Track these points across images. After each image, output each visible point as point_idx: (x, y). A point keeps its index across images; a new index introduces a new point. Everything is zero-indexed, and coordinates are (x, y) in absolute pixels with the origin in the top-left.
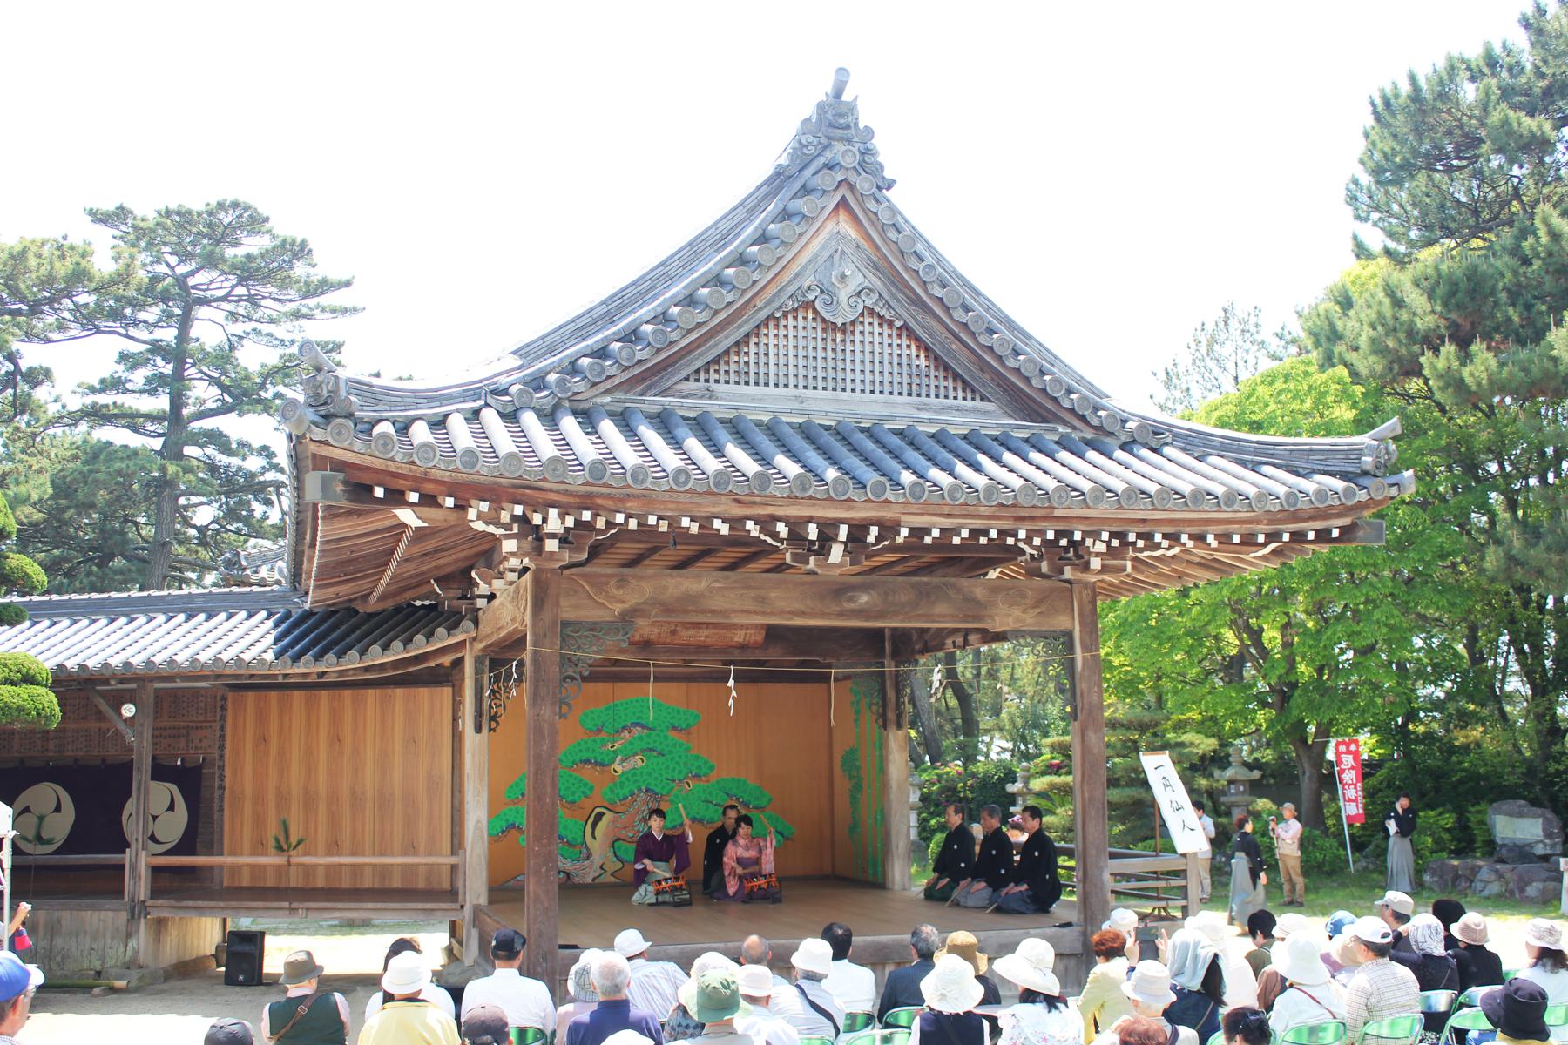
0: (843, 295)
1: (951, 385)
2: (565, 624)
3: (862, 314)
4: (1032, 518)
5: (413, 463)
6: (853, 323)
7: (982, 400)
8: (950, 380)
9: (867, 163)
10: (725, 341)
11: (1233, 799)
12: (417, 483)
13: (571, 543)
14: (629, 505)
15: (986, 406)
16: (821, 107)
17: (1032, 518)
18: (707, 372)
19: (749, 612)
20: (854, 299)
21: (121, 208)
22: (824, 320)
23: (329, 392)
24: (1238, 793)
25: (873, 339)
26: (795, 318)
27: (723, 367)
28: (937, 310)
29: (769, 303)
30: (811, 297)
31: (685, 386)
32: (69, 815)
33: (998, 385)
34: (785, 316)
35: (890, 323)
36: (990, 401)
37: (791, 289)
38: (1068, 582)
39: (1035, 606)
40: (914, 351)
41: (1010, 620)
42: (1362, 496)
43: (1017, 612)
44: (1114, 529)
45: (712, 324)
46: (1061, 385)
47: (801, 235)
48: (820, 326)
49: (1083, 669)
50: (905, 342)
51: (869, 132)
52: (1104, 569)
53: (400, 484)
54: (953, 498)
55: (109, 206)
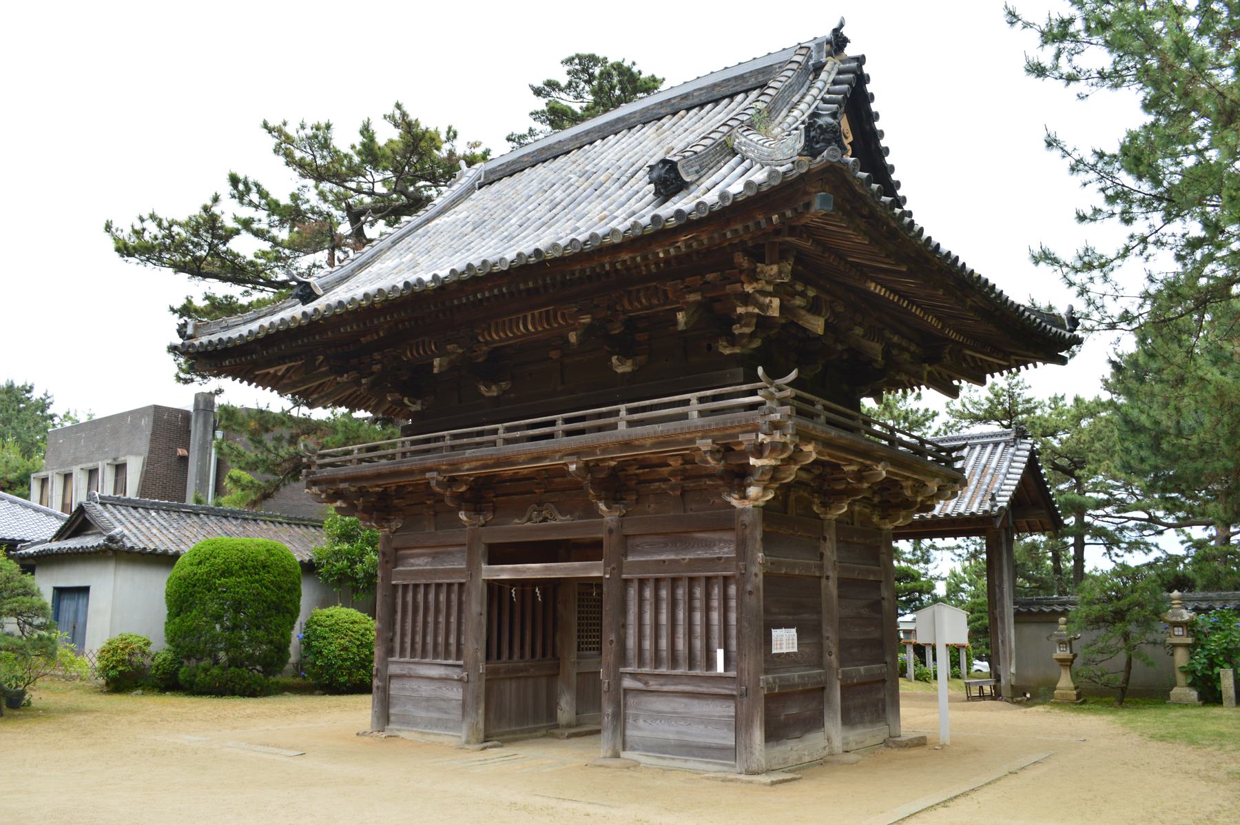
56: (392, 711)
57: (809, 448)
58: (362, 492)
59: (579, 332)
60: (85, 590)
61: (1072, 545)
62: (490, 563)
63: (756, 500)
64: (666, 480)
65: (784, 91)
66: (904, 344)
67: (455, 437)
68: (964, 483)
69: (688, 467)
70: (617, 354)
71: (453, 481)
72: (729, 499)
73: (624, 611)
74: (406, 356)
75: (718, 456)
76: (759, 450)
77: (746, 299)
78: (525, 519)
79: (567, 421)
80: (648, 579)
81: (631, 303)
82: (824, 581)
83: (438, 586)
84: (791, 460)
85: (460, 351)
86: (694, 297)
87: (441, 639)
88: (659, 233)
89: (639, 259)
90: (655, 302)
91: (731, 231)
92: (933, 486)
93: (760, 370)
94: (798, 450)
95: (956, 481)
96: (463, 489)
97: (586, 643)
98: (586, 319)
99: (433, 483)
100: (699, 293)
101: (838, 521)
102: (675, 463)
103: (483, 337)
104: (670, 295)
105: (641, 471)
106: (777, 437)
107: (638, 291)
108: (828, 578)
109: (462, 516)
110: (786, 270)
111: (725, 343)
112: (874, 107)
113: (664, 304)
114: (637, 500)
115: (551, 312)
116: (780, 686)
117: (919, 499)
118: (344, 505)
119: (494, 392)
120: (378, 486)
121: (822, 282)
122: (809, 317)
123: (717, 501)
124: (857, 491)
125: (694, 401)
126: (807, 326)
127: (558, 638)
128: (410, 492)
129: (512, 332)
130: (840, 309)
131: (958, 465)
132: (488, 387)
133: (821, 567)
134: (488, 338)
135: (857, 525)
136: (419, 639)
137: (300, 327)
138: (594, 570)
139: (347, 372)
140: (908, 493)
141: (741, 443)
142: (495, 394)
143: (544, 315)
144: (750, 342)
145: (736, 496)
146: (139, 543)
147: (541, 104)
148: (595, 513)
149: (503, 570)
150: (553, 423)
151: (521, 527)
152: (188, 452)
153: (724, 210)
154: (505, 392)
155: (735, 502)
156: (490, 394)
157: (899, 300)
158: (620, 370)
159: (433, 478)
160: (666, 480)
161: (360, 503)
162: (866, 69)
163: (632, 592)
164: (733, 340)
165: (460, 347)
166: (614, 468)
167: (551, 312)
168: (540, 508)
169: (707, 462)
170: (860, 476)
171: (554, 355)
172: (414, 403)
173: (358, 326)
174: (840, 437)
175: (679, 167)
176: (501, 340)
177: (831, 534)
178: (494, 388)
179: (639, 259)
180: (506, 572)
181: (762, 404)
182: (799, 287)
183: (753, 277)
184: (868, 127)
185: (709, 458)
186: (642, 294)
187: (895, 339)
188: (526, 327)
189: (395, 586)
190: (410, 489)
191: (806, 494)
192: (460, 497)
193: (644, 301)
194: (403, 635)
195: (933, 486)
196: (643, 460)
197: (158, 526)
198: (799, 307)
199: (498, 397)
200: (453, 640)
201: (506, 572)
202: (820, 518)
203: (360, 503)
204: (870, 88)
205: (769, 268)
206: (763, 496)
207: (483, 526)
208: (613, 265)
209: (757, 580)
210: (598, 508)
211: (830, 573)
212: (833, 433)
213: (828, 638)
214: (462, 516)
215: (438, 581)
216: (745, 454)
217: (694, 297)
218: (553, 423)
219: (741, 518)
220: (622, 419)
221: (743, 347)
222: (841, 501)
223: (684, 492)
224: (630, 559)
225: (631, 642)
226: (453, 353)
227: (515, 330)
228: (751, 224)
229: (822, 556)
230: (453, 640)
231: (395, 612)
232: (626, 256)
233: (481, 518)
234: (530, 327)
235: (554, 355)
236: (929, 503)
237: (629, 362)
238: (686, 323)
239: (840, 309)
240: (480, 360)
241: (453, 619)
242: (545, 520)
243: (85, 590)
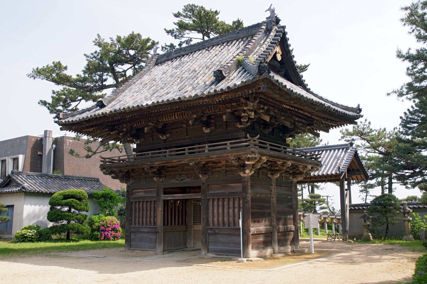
56: (132, 243)
57: (264, 158)
58: (120, 171)
59: (192, 121)
60: (13, 206)
61: (387, 183)
62: (164, 194)
63: (248, 174)
64: (220, 167)
65: (258, 40)
66: (300, 120)
67: (152, 154)
68: (321, 166)
69: (227, 163)
70: (205, 127)
71: (152, 167)
72: (240, 174)
73: (208, 209)
74: (134, 126)
75: (236, 161)
76: (248, 159)
77: (244, 111)
78: (176, 180)
79: (189, 149)
80: (215, 199)
81: (209, 111)
82: (272, 199)
83: (147, 202)
84: (259, 161)
85: (153, 125)
86: (229, 110)
87: (148, 220)
88: (216, 94)
89: (210, 101)
90: (217, 111)
91: (238, 95)
92: (309, 167)
93: (248, 135)
94: (260, 158)
95: (319, 165)
96: (155, 170)
97: (196, 214)
98: (195, 116)
99: (145, 169)
100: (230, 109)
101: (277, 179)
102: (224, 163)
103: (161, 120)
104: (221, 109)
105: (213, 164)
106: (253, 156)
107: (211, 107)
108: (273, 198)
109: (155, 179)
110: (255, 105)
111: (239, 124)
112: (289, 42)
113: (219, 112)
114: (212, 174)
115: (183, 113)
116: (256, 231)
117: (305, 171)
118: (114, 176)
119: (164, 138)
120: (126, 169)
121: (270, 104)
122: (265, 116)
123: (236, 174)
124: (282, 170)
125: (228, 144)
126: (264, 119)
127: (186, 219)
128: (137, 171)
129: (170, 118)
130: (277, 111)
131: (320, 160)
132: (163, 136)
133: (271, 194)
134: (162, 121)
135: (284, 180)
136: (141, 220)
137: (101, 117)
138: (198, 196)
139: (114, 131)
140: (301, 169)
141: (242, 157)
142: (165, 138)
143: (181, 114)
144: (247, 124)
145: (242, 173)
146: (37, 189)
147: (177, 20)
148: (199, 178)
149: (169, 196)
150: (184, 150)
151: (174, 182)
152: (42, 153)
153: (235, 89)
154: (168, 138)
155: (242, 175)
156: (163, 138)
157: (294, 109)
158: (206, 132)
159: (145, 167)
160: (220, 167)
161: (120, 175)
162: (286, 30)
163: (211, 203)
164: (241, 124)
165: (153, 123)
166: (204, 164)
167: (183, 113)
168: (181, 176)
169: (233, 163)
170: (283, 165)
171: (184, 126)
172: (137, 141)
173: (120, 117)
174: (274, 154)
175: (223, 72)
176: (167, 121)
177: (274, 184)
178: (164, 136)
179: (210, 101)
180: (170, 197)
181: (249, 145)
182: (262, 106)
183: (246, 105)
184: (287, 49)
185: (233, 162)
186: (212, 108)
187: (297, 119)
188: (175, 117)
189: (132, 202)
190: (137, 170)
191: (265, 171)
192: (154, 173)
193: (213, 110)
194: (135, 218)
195: (309, 167)
196: (213, 161)
197: (38, 182)
198: (262, 113)
199: (166, 139)
200: (152, 220)
201: (170, 197)
202: (270, 179)
203: (120, 175)
204: (287, 36)
205: (250, 103)
206: (250, 172)
207: (162, 182)
208: (203, 103)
209: (249, 199)
210: (199, 176)
211: (274, 196)
212: (272, 153)
213: (273, 217)
214: (155, 179)
215: (147, 200)
216: (244, 160)
217: (229, 110)
218: (184, 150)
219: (244, 180)
220: (206, 149)
221: (244, 125)
222: (277, 173)
223: (226, 171)
224: (210, 192)
225: (210, 219)
226: (151, 126)
227: (172, 118)
228: (243, 93)
229: (271, 190)
230: (152, 220)
231: (132, 211)
232: (206, 100)
233: (161, 180)
234: (176, 117)
235: (184, 126)
236: (309, 172)
237: (209, 129)
238: (226, 119)
239: (277, 111)
240: (160, 128)
241: (152, 213)
242: (182, 180)
243: (13, 206)
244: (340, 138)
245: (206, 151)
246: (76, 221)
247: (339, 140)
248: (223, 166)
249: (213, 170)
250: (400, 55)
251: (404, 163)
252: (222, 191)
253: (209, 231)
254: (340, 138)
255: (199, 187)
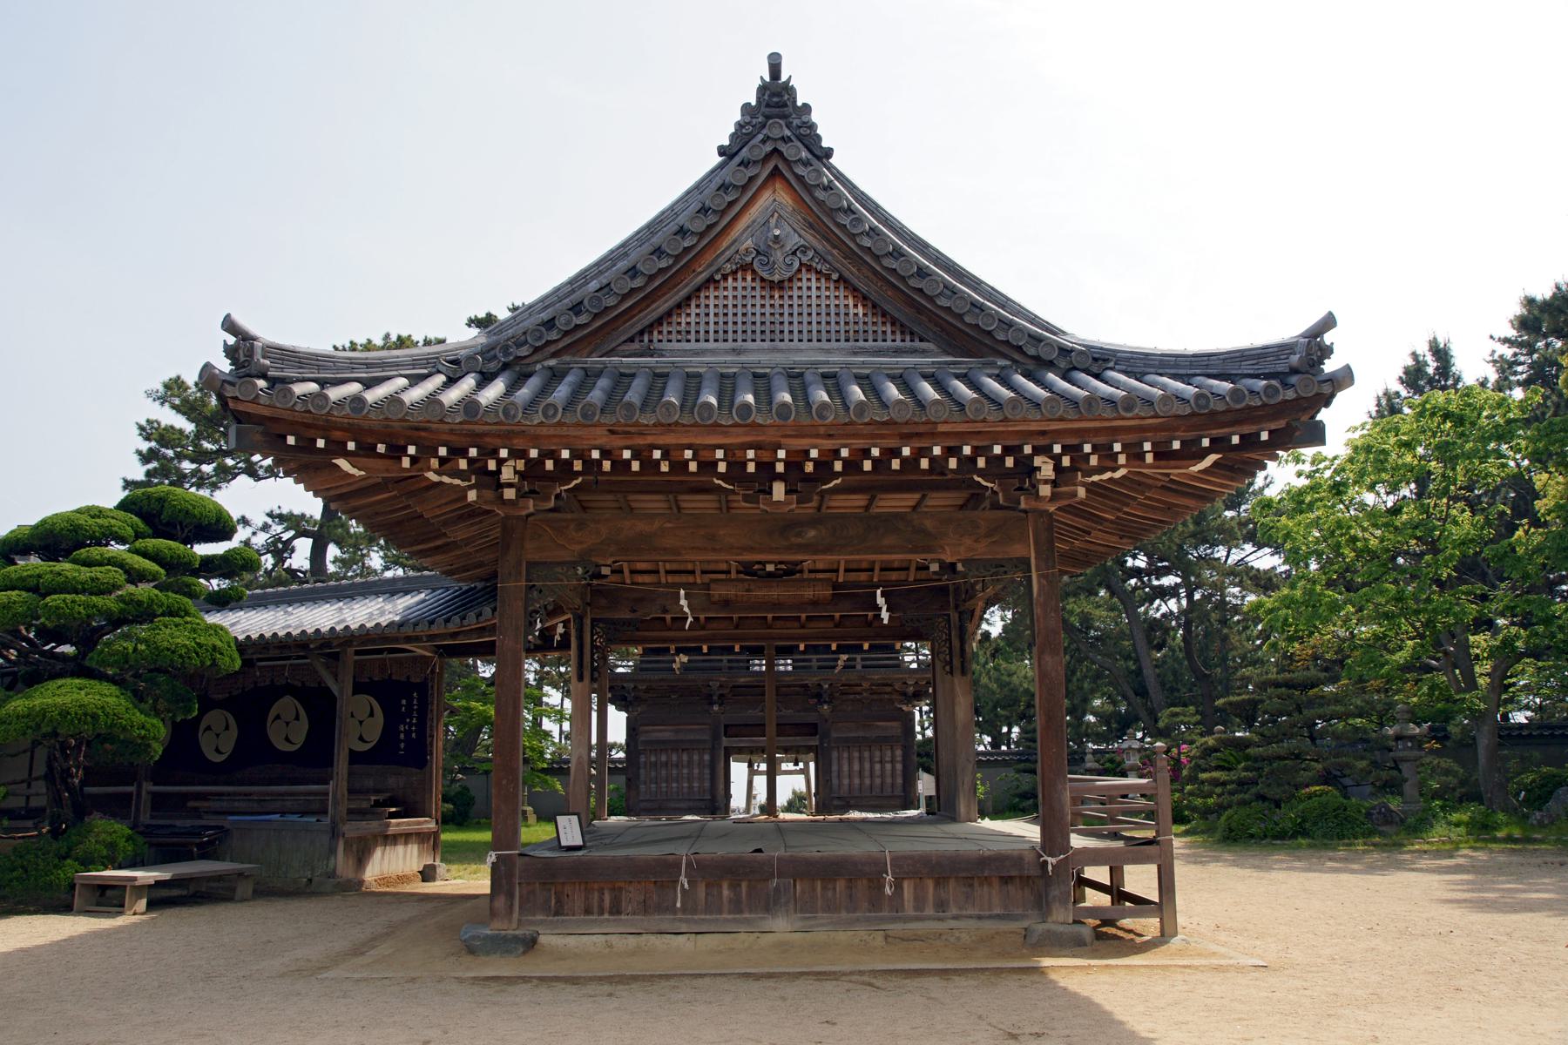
0: (778, 256)
1: (889, 329)
2: (531, 565)
3: (799, 271)
4: (918, 435)
5: (309, 412)
6: (790, 280)
7: (921, 340)
8: (889, 325)
9: (808, 136)
10: (662, 306)
11: (1401, 754)
12: (355, 432)
13: (538, 493)
14: (515, 441)
15: (924, 345)
16: (763, 89)
17: (918, 435)
18: (651, 333)
19: (698, 548)
20: (790, 257)
21: (489, 315)
22: (763, 280)
23: (245, 356)
24: (1406, 748)
25: (813, 292)
26: (735, 279)
27: (665, 328)
28: (868, 259)
29: (710, 265)
30: (749, 259)
31: (624, 347)
32: (234, 733)
33: (936, 325)
34: (725, 278)
35: (828, 278)
36: (929, 341)
37: (728, 253)
38: (1025, 511)
39: (987, 536)
40: (851, 302)
41: (962, 549)
42: (1290, 394)
43: (968, 541)
44: (1009, 443)
45: (649, 289)
46: (994, 318)
47: (731, 204)
48: (757, 284)
49: (1039, 595)
50: (842, 293)
51: (807, 108)
52: (1054, 497)
53: (337, 435)
54: (821, 417)
55: (481, 315)
64: (859, 694)
160: (859, 694)
244: (1496, 337)
245: (859, 667)
246: (284, 869)
247: (1491, 337)
248: (865, 690)
249: (844, 697)
250: (1329, 322)
251: (473, 477)
252: (861, 734)
253: (836, 802)
254: (1496, 337)
255: (815, 726)
